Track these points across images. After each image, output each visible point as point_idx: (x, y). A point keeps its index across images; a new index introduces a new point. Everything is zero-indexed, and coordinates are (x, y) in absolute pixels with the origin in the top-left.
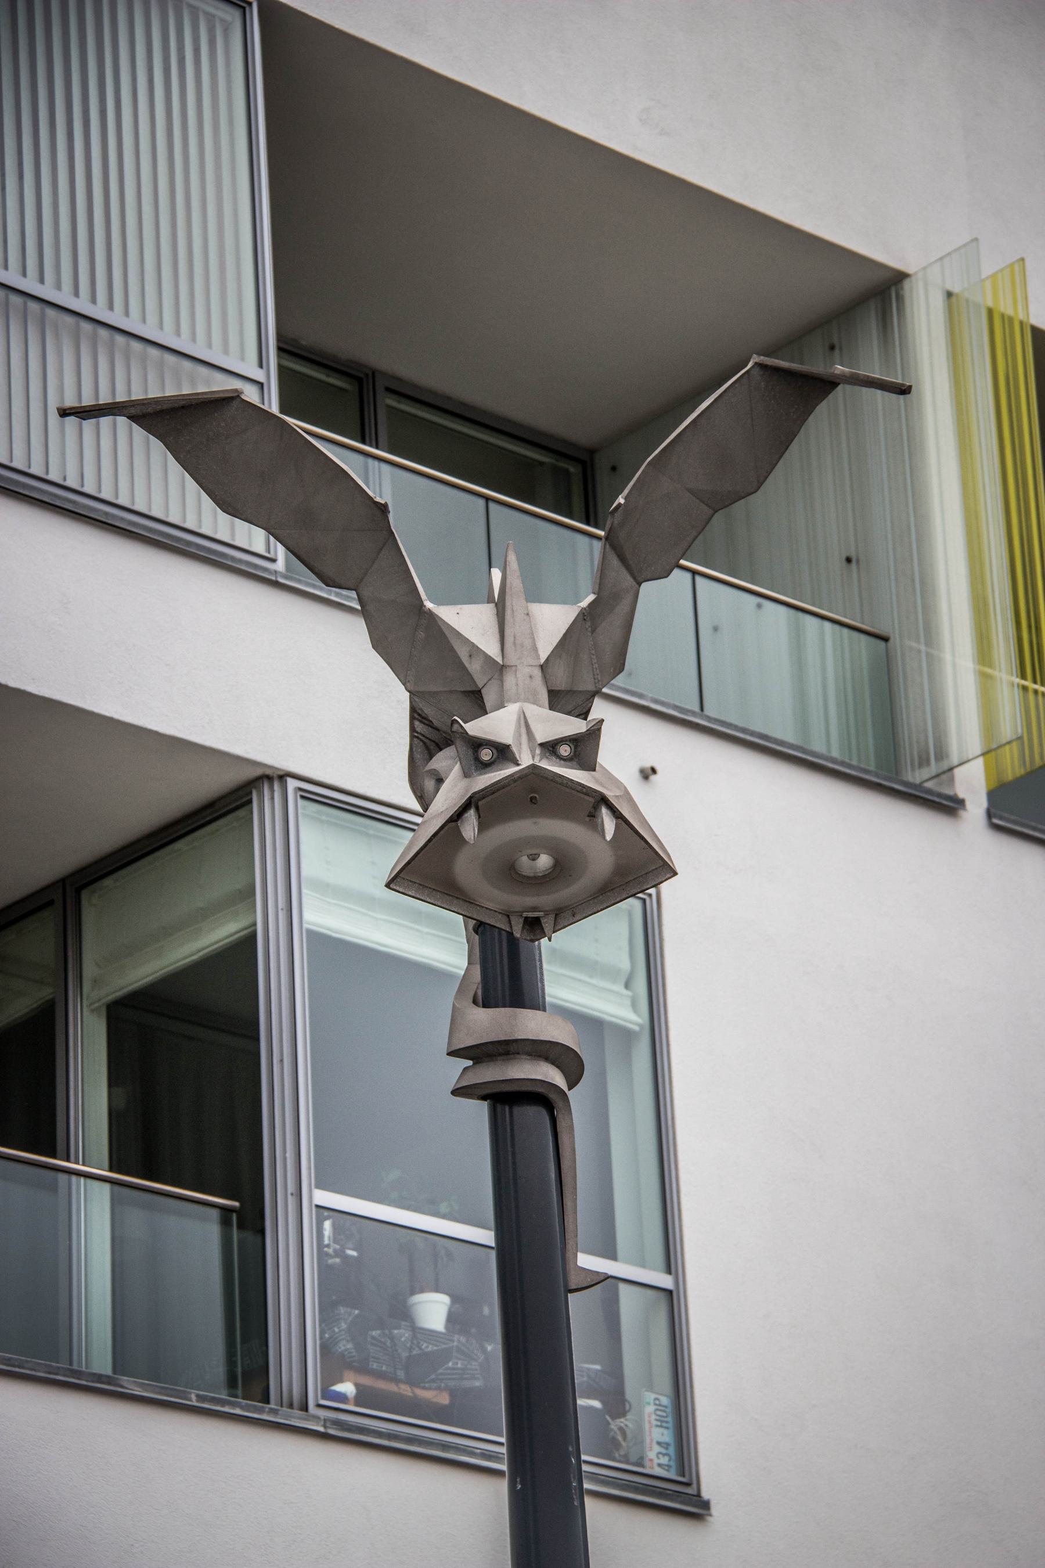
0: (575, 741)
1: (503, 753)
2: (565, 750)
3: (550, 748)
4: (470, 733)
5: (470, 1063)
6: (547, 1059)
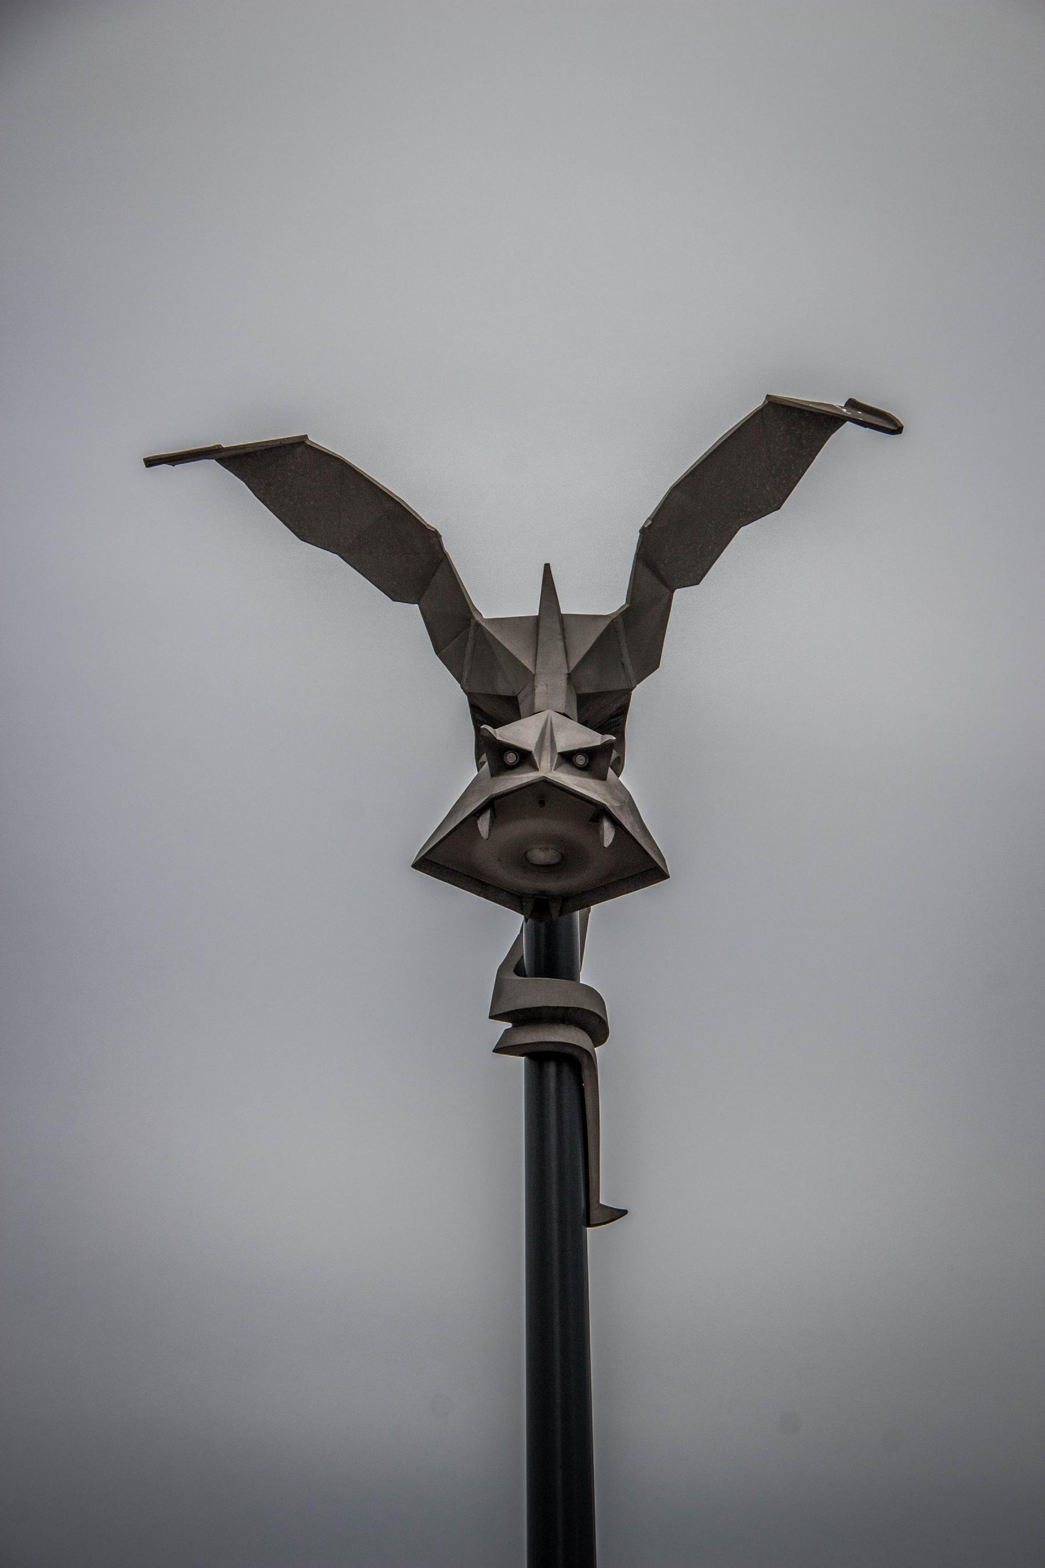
0: (590, 753)
1: (525, 758)
2: (581, 760)
3: (567, 758)
4: (498, 738)
5: (509, 1025)
6: (583, 1028)
